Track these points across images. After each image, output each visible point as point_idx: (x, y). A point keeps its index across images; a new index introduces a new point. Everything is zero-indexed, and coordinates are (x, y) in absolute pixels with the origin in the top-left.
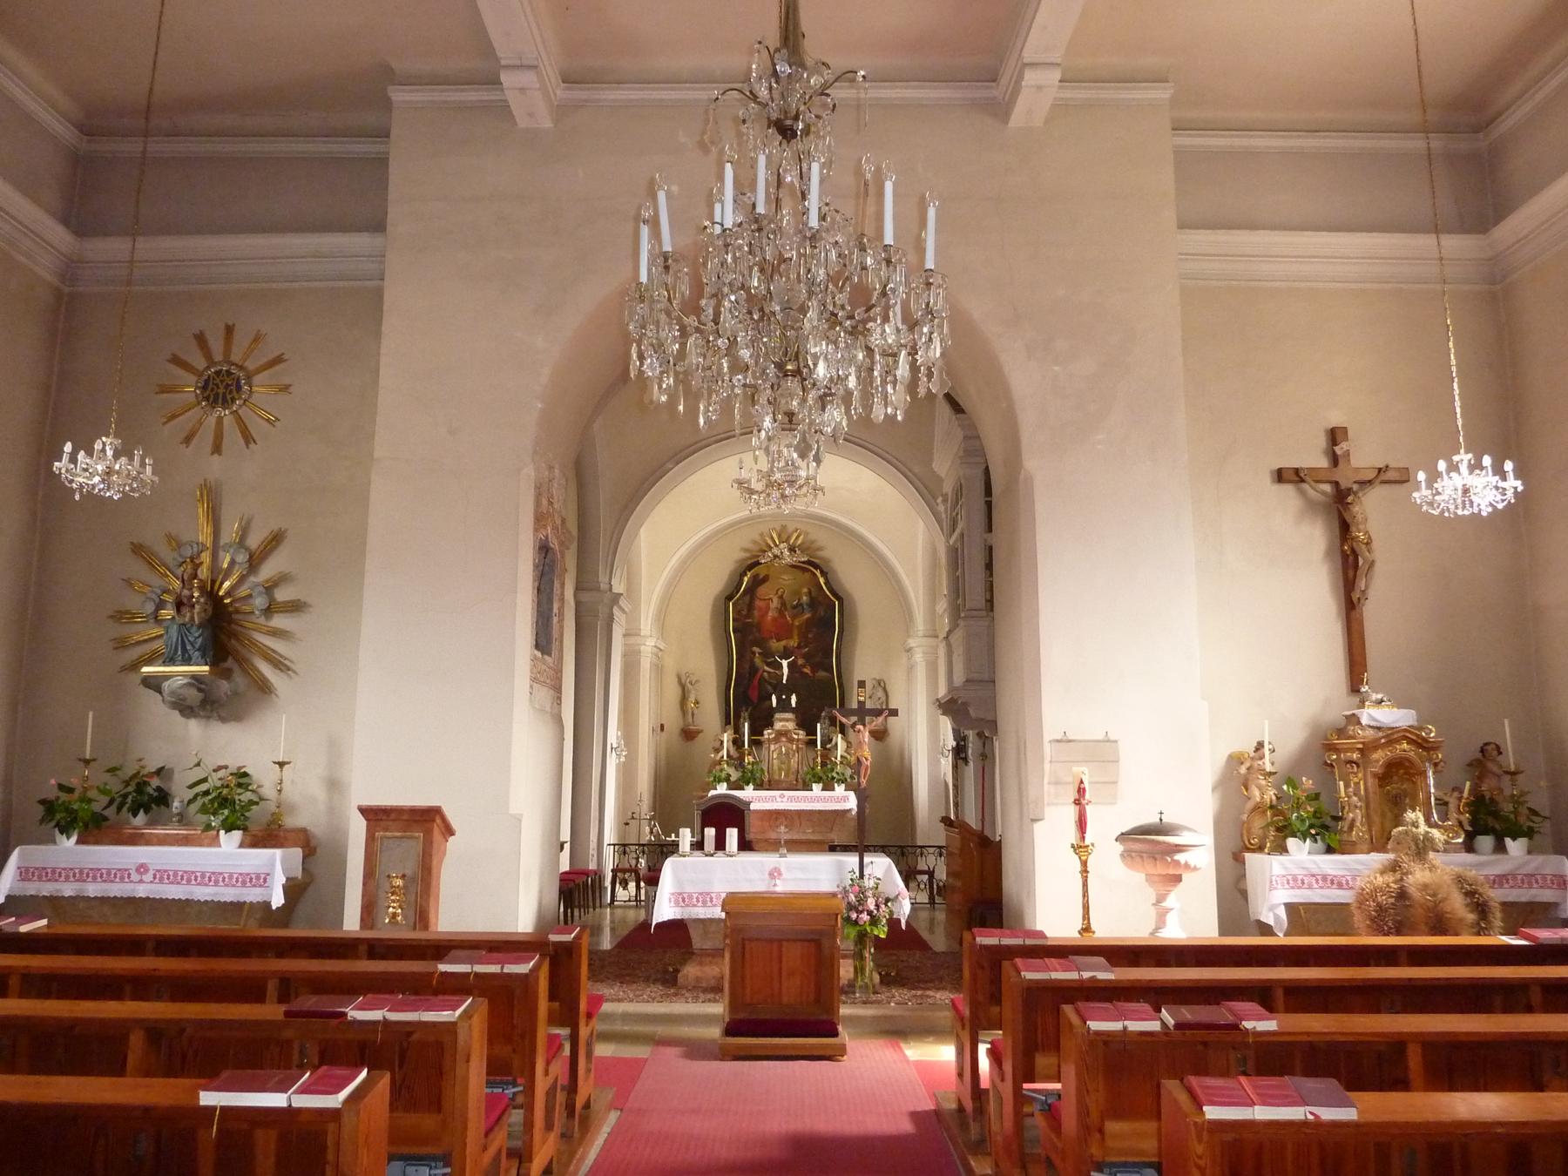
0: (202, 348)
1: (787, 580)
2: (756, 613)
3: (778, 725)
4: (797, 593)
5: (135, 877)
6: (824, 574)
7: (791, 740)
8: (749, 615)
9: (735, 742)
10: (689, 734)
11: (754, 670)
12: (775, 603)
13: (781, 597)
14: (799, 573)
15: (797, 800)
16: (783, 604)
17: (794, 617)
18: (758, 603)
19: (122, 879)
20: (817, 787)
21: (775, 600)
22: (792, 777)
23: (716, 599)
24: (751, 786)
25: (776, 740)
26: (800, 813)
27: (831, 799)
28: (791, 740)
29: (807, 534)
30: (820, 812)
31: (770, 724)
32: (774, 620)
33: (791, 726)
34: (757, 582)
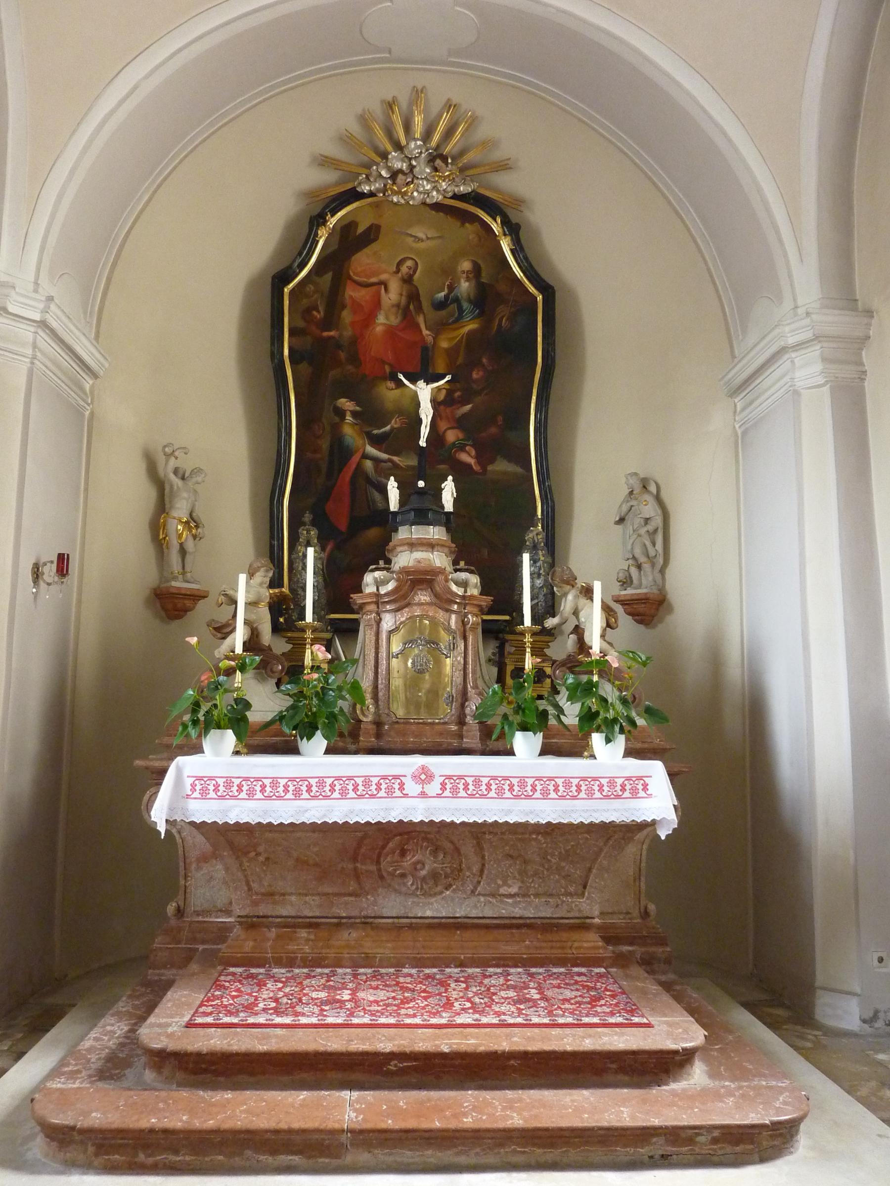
0: (559, 959)
1: (424, 238)
2: (347, 316)
3: (404, 559)
4: (448, 271)
5: (412, 788)
6: (513, 229)
7: (444, 601)
8: (330, 321)
9: (277, 607)
10: (171, 604)
11: (341, 452)
12: (393, 294)
13: (408, 280)
14: (452, 223)
15: (477, 788)
16: (413, 297)
17: (439, 328)
18: (351, 293)
19: (390, 792)
20: (525, 744)
21: (395, 286)
22: (446, 711)
23: (253, 286)
24: (319, 742)
25: (401, 599)
26: (479, 832)
27: (571, 789)
28: (444, 601)
29: (473, 122)
30: (550, 830)
31: (379, 555)
32: (390, 332)
33: (439, 560)
34: (350, 241)
